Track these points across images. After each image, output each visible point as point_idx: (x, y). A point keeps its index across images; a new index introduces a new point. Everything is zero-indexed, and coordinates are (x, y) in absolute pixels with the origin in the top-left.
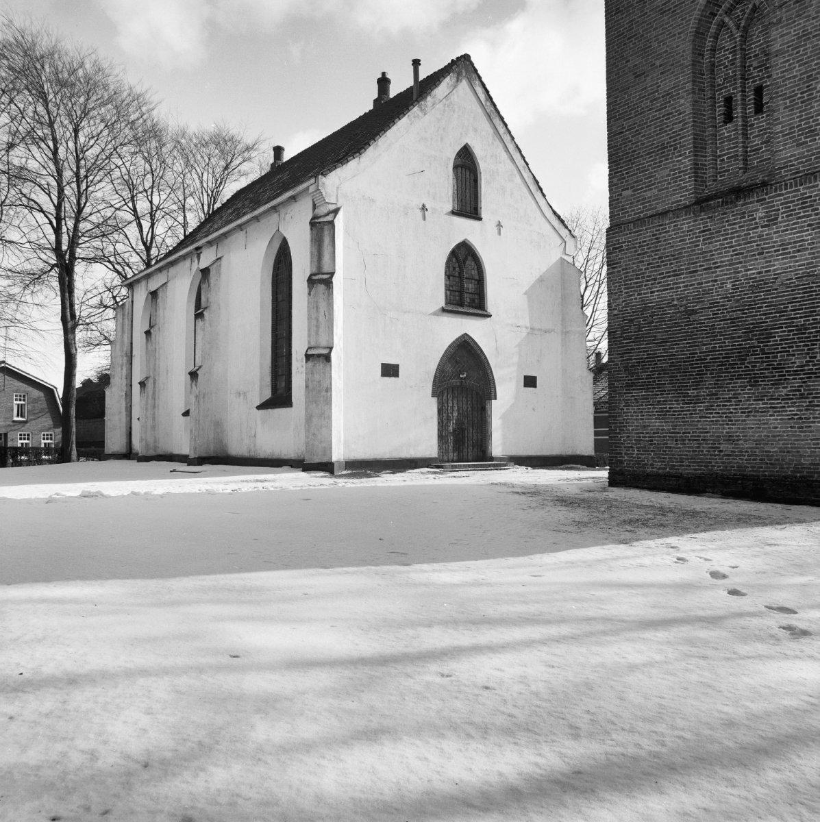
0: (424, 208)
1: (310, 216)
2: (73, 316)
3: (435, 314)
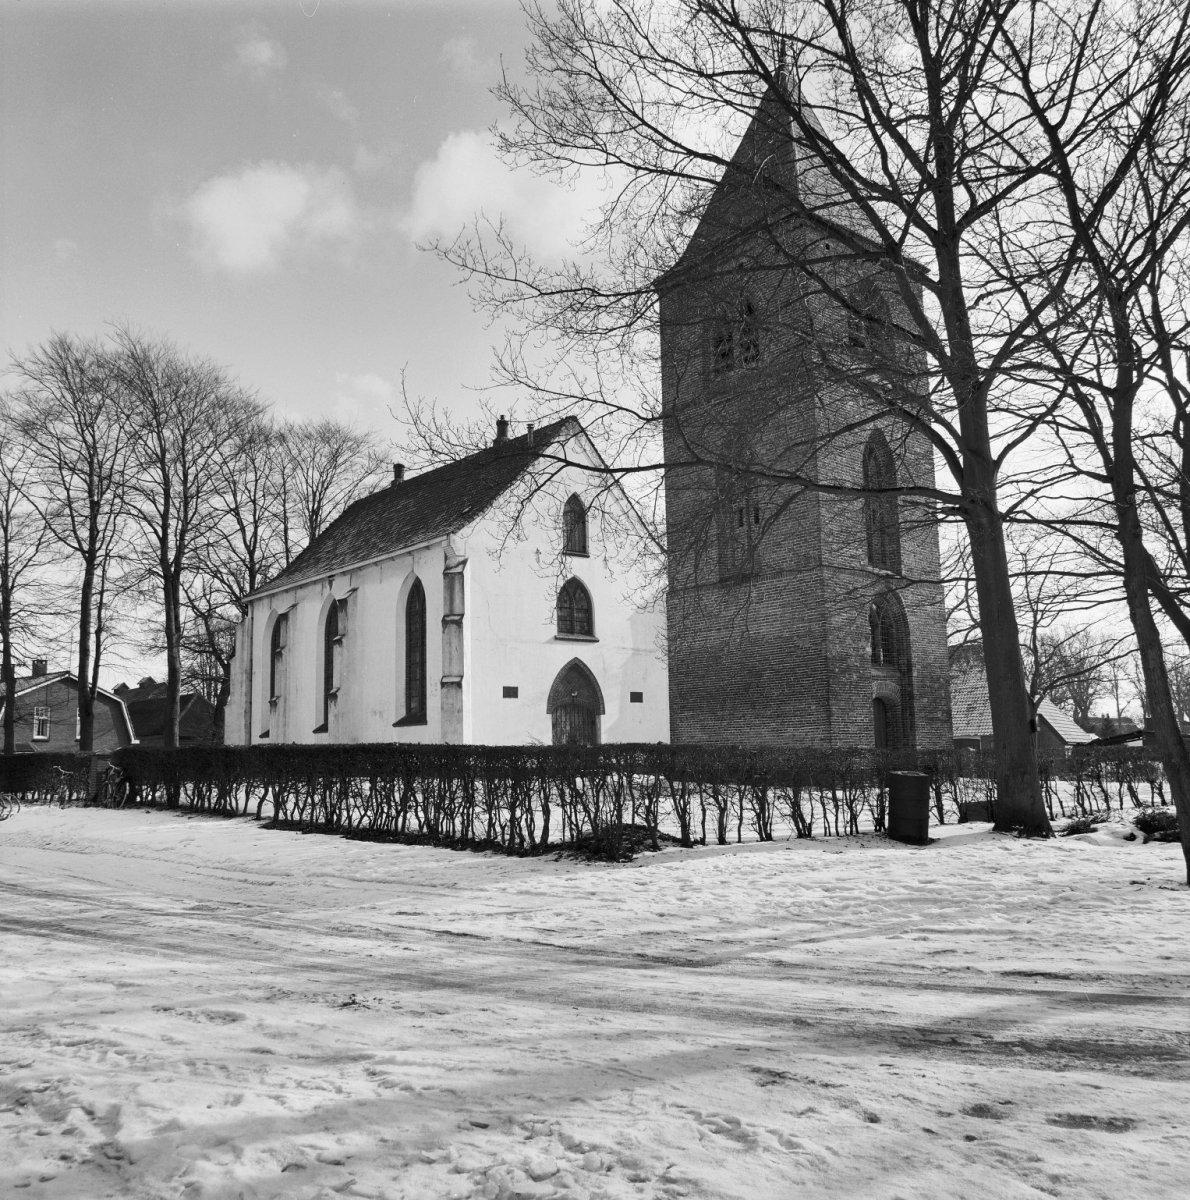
0: (538, 552)
1: (443, 568)
3: (548, 642)
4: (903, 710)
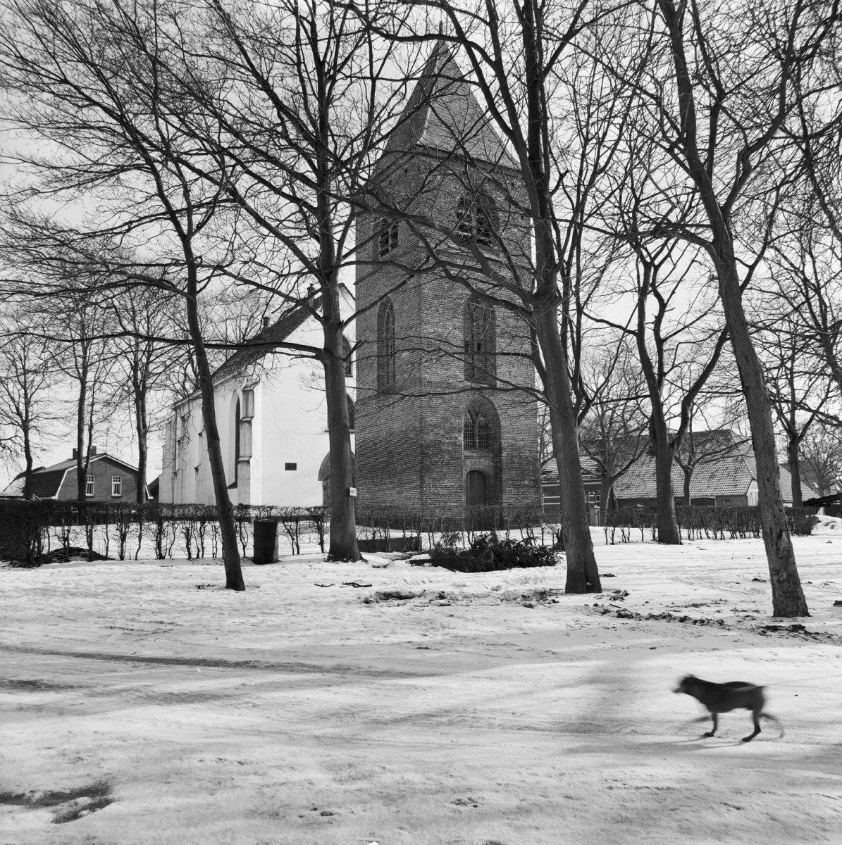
2: (145, 426)
3: (320, 434)
4: (496, 479)
